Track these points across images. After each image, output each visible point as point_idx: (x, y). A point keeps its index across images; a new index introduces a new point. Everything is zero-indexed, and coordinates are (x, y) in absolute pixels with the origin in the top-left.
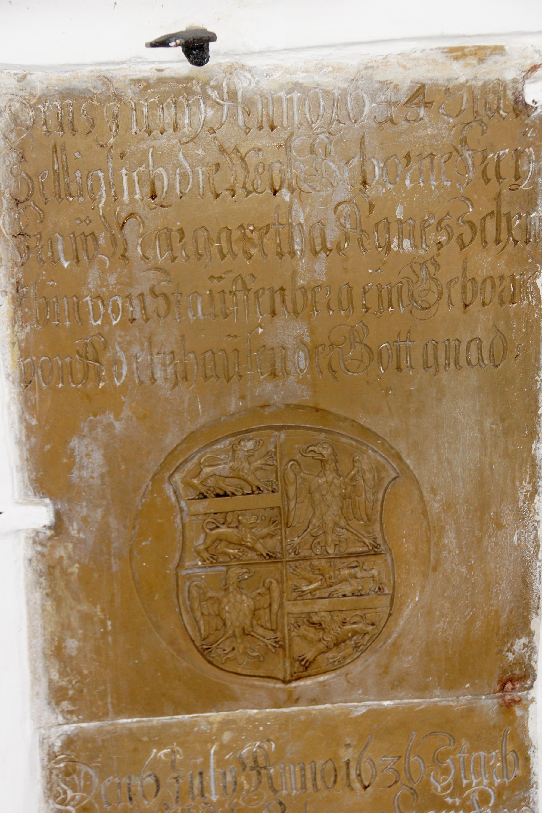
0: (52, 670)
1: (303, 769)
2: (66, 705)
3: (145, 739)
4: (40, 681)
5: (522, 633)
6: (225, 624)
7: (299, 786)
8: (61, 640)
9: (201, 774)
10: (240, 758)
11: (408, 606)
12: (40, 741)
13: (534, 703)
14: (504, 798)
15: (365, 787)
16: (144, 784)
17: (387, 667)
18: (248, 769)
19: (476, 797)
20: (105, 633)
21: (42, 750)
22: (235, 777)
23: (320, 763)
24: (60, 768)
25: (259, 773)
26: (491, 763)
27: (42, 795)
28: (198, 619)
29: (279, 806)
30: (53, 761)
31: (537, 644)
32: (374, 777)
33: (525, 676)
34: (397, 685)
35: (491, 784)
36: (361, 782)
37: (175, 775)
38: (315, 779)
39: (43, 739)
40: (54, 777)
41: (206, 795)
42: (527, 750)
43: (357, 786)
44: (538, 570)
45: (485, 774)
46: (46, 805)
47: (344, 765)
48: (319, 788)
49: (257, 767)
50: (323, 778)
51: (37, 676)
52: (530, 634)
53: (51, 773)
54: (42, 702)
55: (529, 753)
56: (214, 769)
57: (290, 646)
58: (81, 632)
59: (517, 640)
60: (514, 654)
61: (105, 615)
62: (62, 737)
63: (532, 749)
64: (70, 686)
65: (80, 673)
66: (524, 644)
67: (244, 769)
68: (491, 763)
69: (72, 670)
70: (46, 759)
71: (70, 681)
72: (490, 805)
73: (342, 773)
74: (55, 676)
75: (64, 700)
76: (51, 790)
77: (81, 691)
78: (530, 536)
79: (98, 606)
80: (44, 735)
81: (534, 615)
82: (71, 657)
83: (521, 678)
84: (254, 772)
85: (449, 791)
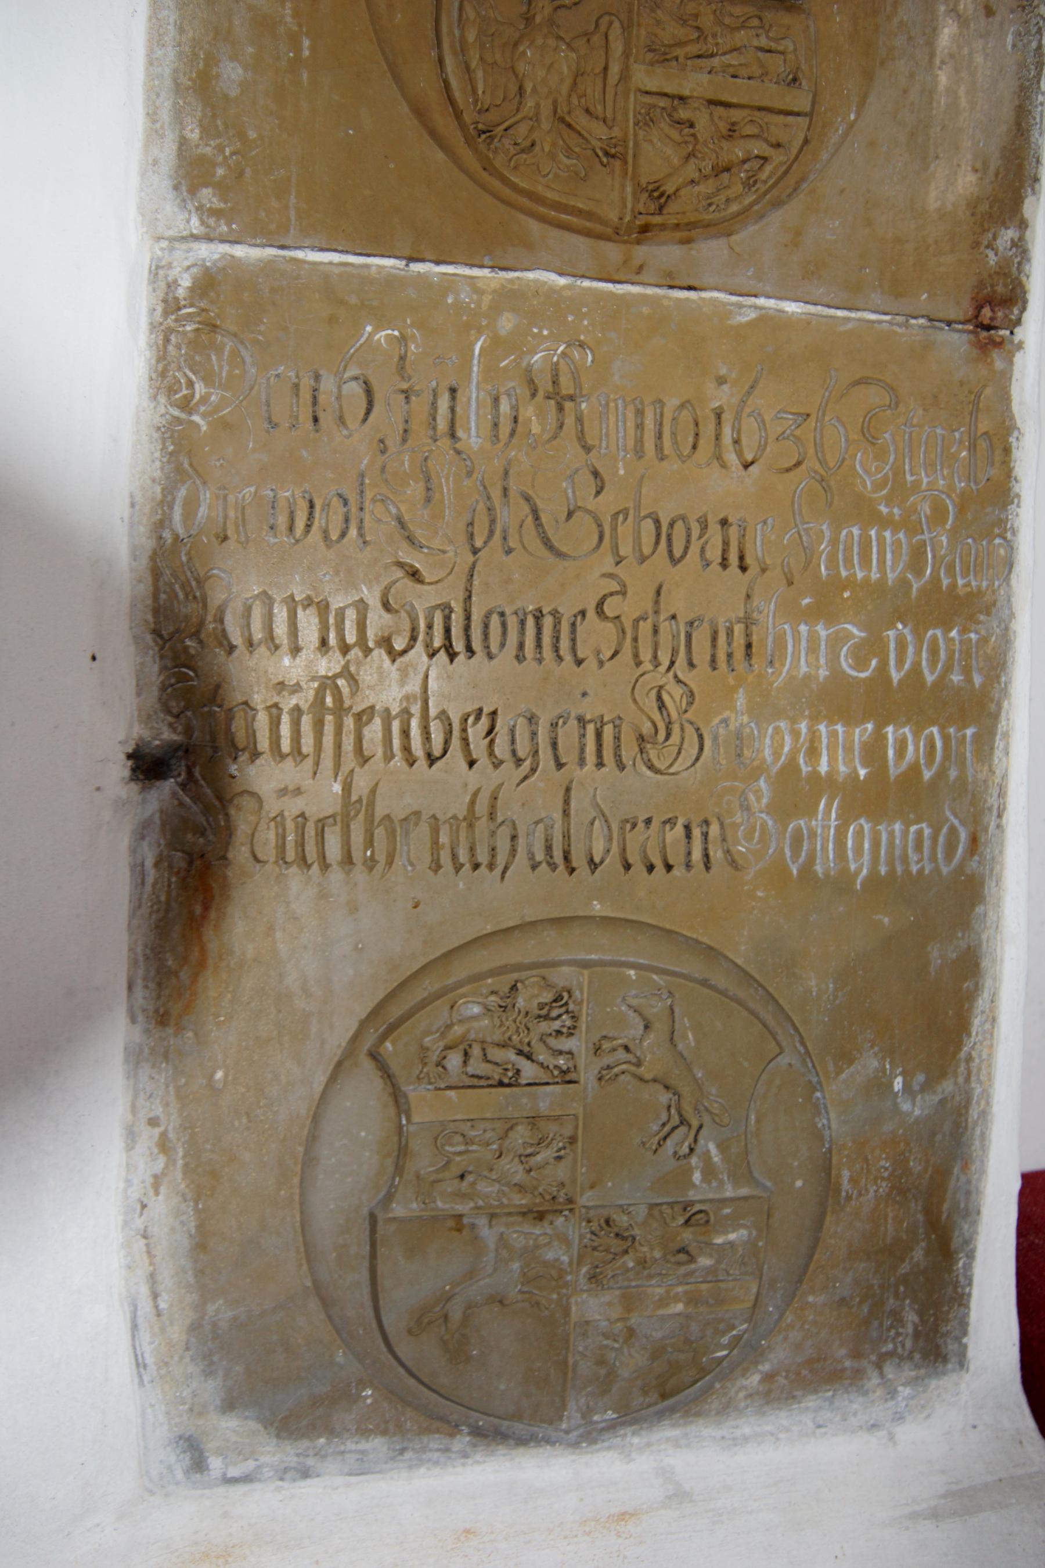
0: (189, 119)
1: (640, 413)
2: (206, 194)
3: (353, 300)
4: (162, 136)
5: (1010, 219)
6: (521, 90)
7: (631, 443)
8: (211, 60)
9: (453, 391)
10: (529, 369)
11: (837, 130)
12: (150, 272)
13: (1022, 351)
14: (969, 516)
15: (746, 466)
16: (344, 392)
17: (798, 233)
18: (541, 394)
19: (926, 508)
20: (296, 63)
21: (154, 290)
22: (515, 408)
23: (672, 403)
24: (185, 333)
25: (560, 409)
26: (953, 450)
27: (145, 383)
28: (473, 65)
29: (592, 478)
30: (173, 317)
31: (1030, 246)
32: (762, 448)
33: (1011, 300)
34: (813, 273)
35: (951, 487)
36: (740, 454)
37: (405, 386)
38: (660, 436)
39: (158, 267)
40: (170, 348)
41: (460, 433)
42: (1009, 434)
43: (732, 458)
44: (1039, 109)
45: (942, 469)
46: (152, 405)
47: (712, 416)
48: (666, 452)
49: (560, 400)
50: (674, 434)
51: (158, 125)
52: (1023, 225)
53: (167, 340)
54: (162, 183)
55: (1011, 439)
56: (478, 383)
57: (634, 156)
58: (250, 50)
59: (1003, 229)
60: (996, 255)
61: (300, 26)
62: (195, 270)
63: (1016, 434)
64: (220, 159)
65: (242, 135)
66: (1012, 240)
67: (534, 395)
68: (953, 450)
69: (227, 127)
70: (159, 310)
71: (220, 149)
72: (948, 527)
73: (708, 430)
74: (194, 135)
75: (206, 185)
76: (163, 374)
77: (241, 174)
78: (1030, 42)
79: (288, 5)
80: (160, 259)
81: (1029, 190)
82: (226, 97)
83: (1005, 301)
84: (552, 402)
85: (884, 492)
